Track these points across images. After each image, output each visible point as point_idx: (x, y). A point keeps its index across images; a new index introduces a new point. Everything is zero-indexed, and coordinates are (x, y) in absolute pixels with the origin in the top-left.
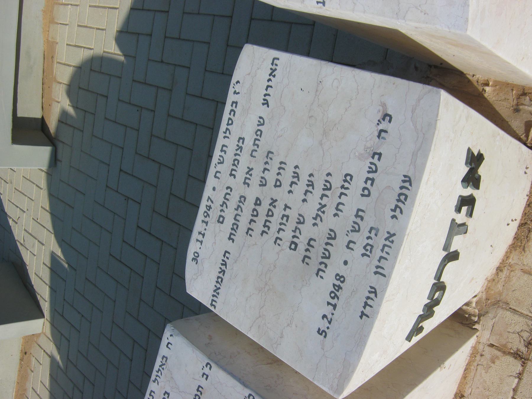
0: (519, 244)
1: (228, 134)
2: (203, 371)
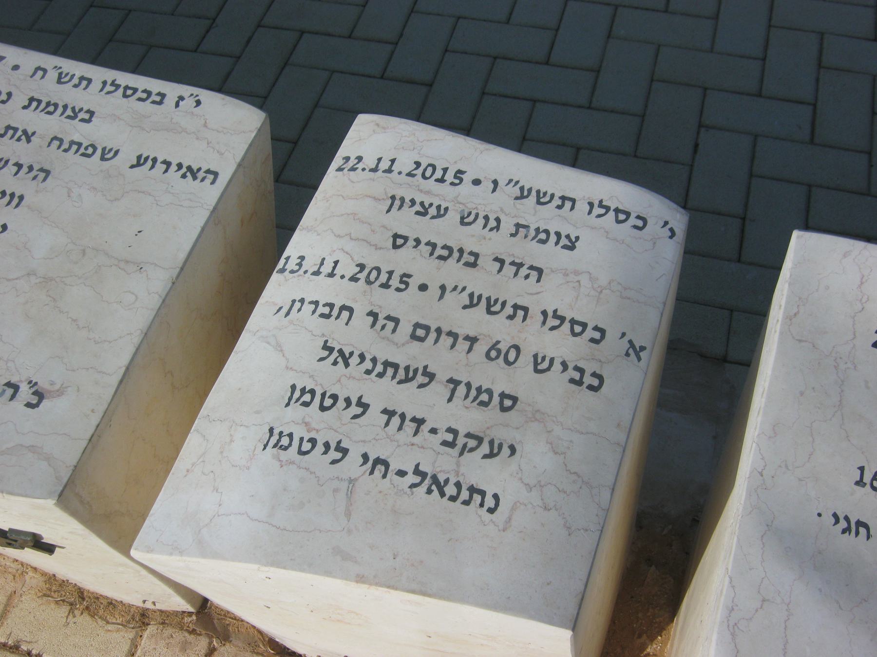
0: (54, 588)
1: (109, 88)
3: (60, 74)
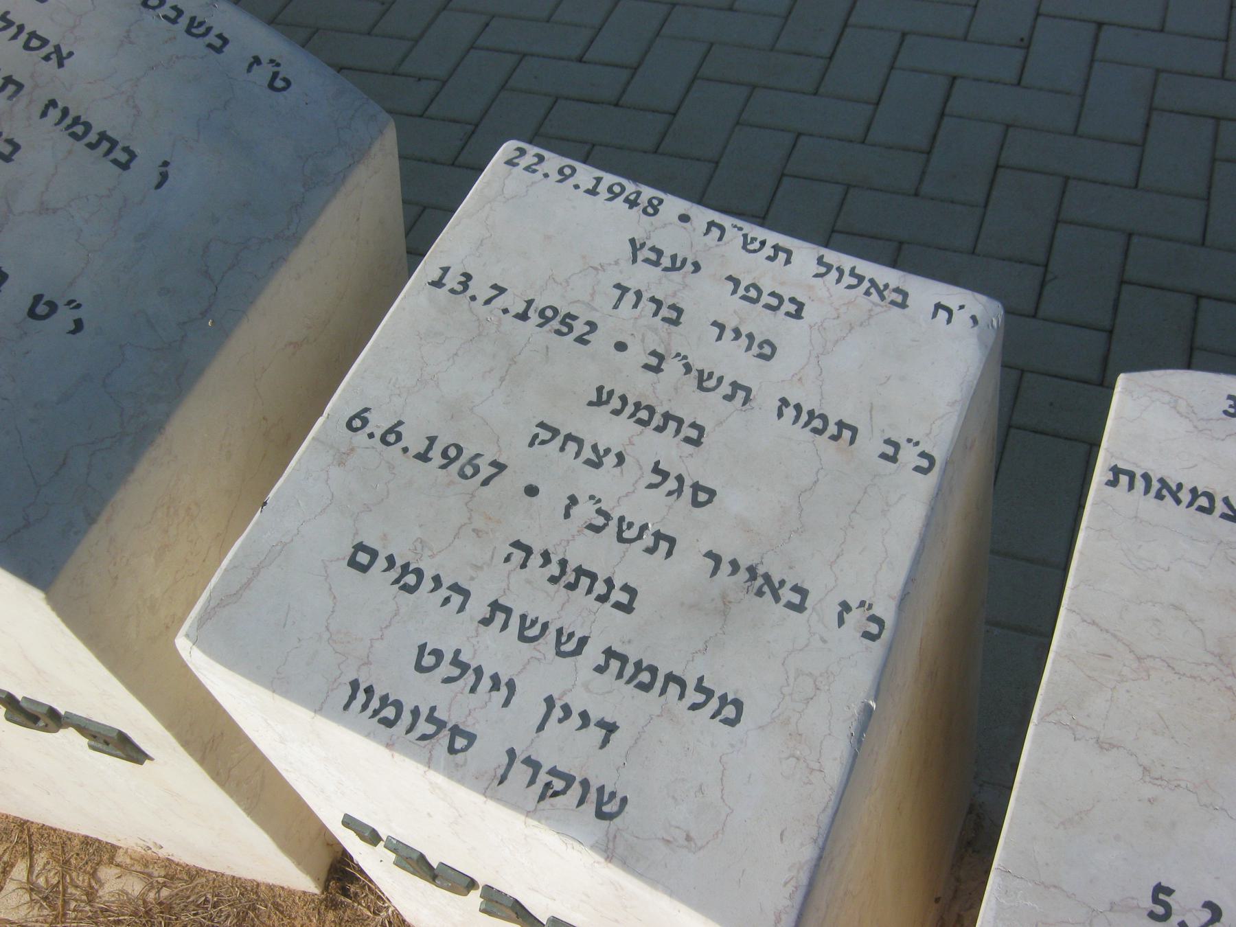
2: (903, 443)
3: (275, 75)
